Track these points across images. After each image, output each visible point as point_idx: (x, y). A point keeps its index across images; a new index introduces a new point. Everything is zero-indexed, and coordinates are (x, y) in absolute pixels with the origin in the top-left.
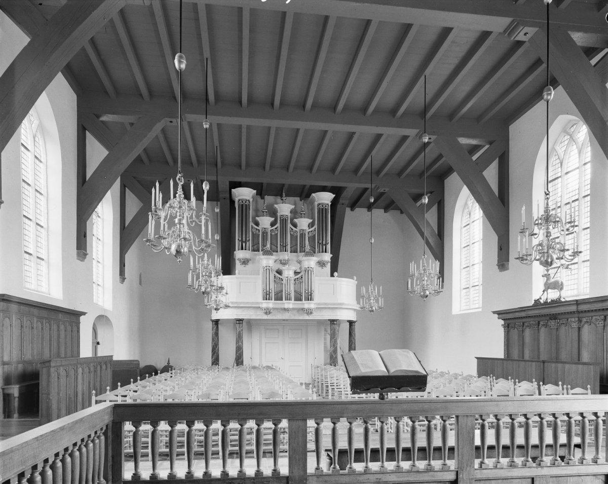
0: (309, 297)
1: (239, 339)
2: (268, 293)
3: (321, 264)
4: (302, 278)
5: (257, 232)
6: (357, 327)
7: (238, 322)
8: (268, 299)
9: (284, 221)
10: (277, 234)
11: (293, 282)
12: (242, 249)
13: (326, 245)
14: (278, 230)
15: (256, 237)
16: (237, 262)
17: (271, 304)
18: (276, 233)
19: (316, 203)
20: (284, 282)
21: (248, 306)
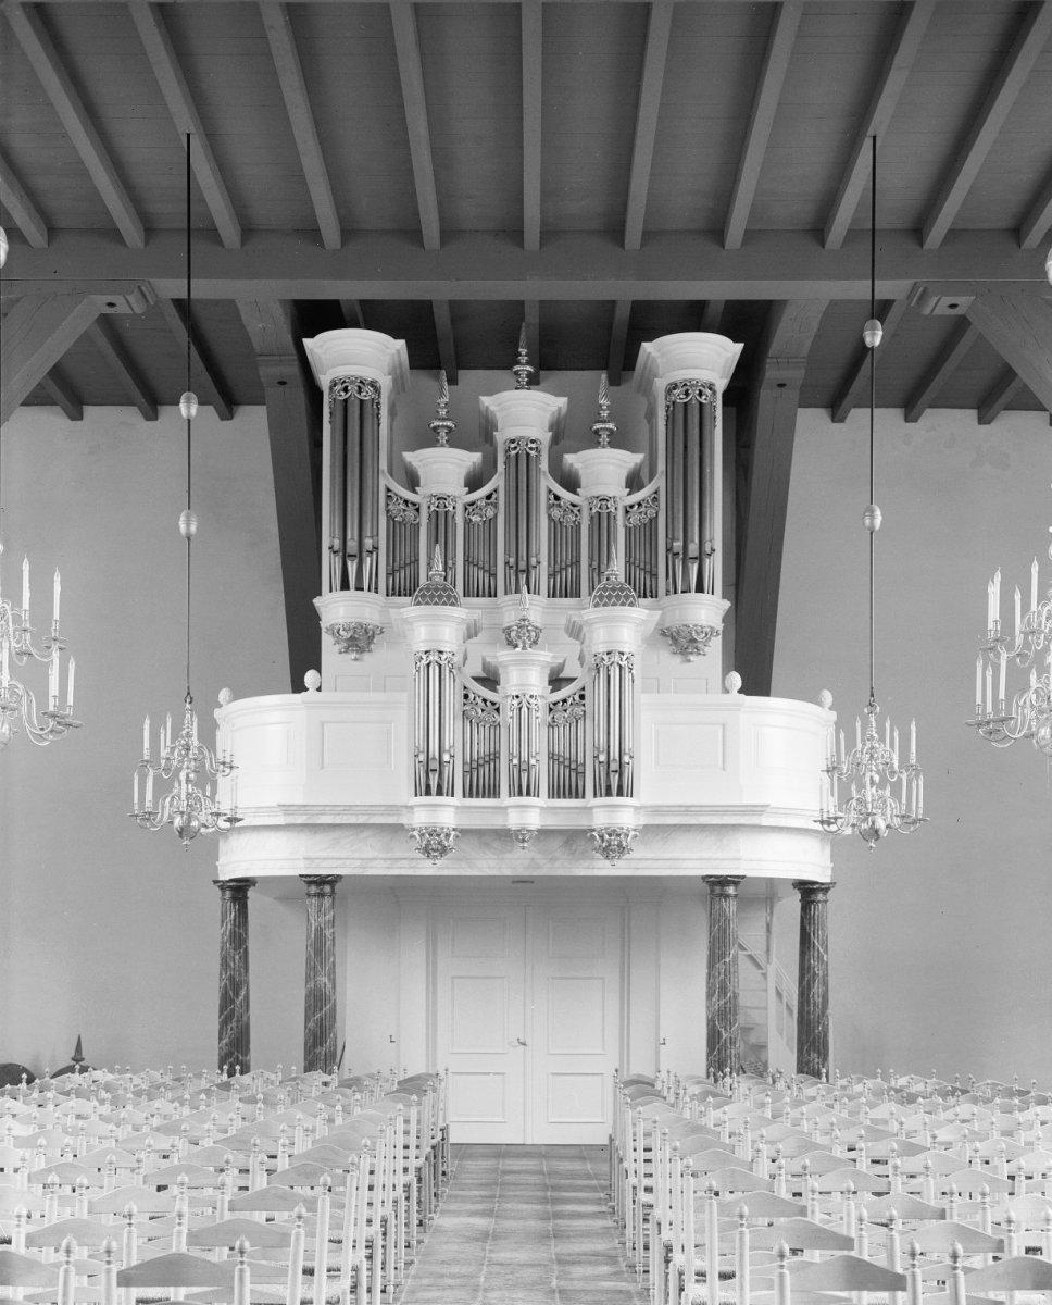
0: (616, 782)
1: (320, 953)
2: (434, 765)
3: (681, 641)
4: (582, 697)
5: (411, 514)
6: (835, 916)
7: (313, 889)
8: (434, 789)
9: (521, 462)
10: (492, 521)
11: (541, 716)
12: (345, 586)
13: (700, 559)
14: (496, 506)
15: (403, 533)
16: (327, 641)
17: (448, 812)
18: (490, 514)
19: (660, 385)
20: (507, 716)
21: (353, 820)
